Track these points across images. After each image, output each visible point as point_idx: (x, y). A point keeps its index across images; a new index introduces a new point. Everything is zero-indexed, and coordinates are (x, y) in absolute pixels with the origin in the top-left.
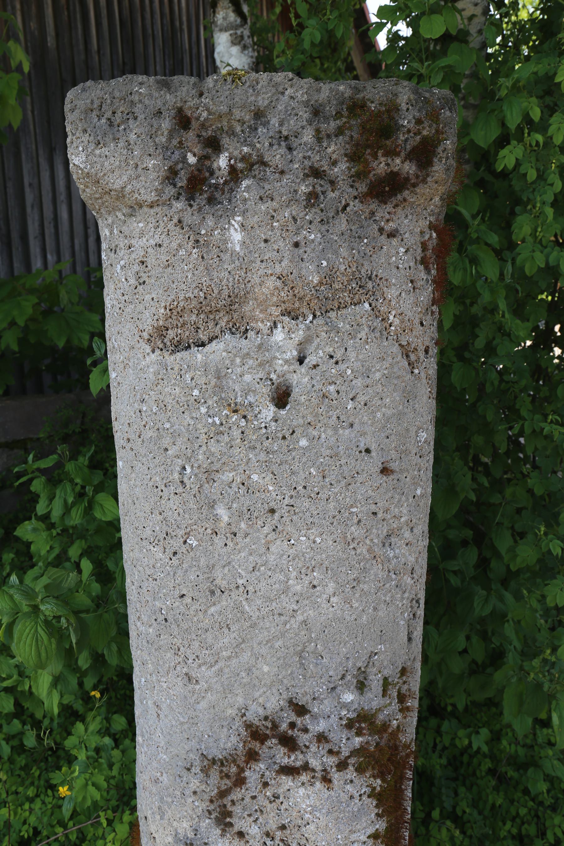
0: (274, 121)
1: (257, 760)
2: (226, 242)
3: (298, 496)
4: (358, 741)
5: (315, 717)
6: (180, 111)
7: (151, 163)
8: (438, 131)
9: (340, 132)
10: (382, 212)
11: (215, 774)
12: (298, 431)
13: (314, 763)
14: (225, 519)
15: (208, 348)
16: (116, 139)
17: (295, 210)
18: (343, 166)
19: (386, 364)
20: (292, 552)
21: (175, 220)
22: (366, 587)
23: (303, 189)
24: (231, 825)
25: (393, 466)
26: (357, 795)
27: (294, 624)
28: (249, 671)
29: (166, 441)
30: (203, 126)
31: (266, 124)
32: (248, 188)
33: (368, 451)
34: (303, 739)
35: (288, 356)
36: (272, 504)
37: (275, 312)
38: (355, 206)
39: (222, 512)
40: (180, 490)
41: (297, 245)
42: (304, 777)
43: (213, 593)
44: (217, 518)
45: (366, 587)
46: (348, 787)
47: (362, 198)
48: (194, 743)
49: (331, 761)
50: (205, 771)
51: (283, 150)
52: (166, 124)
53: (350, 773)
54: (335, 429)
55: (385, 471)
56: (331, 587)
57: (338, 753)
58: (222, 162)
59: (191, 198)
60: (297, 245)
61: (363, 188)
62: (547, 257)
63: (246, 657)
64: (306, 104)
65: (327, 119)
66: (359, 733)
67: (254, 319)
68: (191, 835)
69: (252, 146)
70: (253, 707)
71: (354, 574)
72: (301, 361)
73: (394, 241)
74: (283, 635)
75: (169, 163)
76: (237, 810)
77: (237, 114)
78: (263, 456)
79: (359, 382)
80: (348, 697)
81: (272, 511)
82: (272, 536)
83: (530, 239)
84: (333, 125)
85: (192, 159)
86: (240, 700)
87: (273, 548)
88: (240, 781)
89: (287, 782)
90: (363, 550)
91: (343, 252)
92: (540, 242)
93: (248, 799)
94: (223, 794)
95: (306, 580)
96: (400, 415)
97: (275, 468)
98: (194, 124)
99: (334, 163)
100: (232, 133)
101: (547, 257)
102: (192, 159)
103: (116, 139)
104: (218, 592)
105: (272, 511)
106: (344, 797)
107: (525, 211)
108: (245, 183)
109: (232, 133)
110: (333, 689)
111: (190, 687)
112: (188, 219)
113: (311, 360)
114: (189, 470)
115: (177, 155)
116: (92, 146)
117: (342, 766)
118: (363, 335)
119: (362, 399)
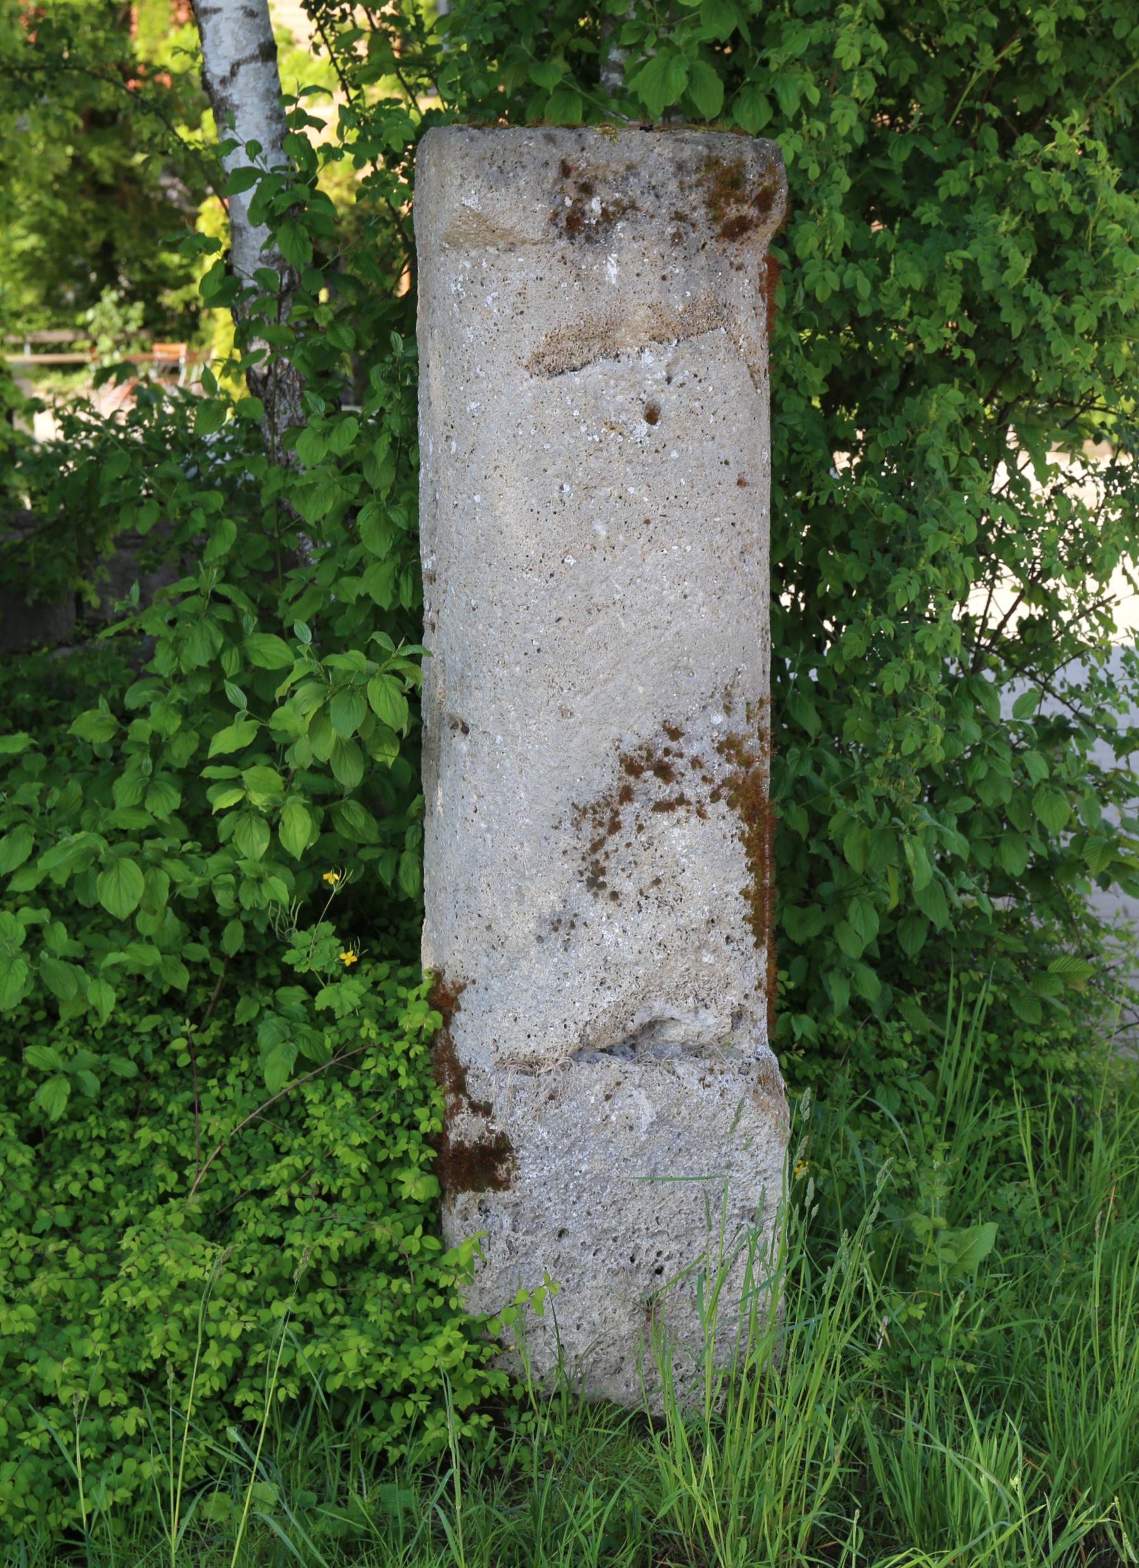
0: (645, 174)
1: (631, 800)
2: (603, 275)
3: (671, 505)
4: (728, 768)
5: (689, 741)
6: (563, 162)
7: (539, 207)
9: (699, 184)
10: (732, 248)
11: (587, 826)
12: (670, 445)
13: (689, 794)
14: (604, 533)
15: (584, 372)
16: (507, 185)
17: (663, 248)
18: (702, 211)
21: (559, 256)
23: (670, 230)
24: (603, 885)
25: (748, 478)
27: (669, 636)
28: (624, 694)
29: (545, 462)
30: (581, 175)
31: (637, 175)
32: (623, 230)
34: (680, 764)
35: (658, 376)
36: (648, 515)
37: (644, 337)
38: (712, 245)
39: (600, 528)
40: (559, 508)
41: (664, 278)
42: (681, 812)
46: (721, 823)
47: (718, 238)
48: (563, 794)
49: (706, 790)
50: (576, 824)
51: (652, 198)
53: (722, 806)
55: (741, 483)
58: (595, 205)
59: (572, 238)
60: (664, 278)
61: (718, 229)
62: (841, 276)
63: (622, 678)
64: (672, 160)
65: (689, 173)
66: (729, 761)
67: (623, 344)
68: (559, 908)
69: (625, 193)
71: (719, 584)
72: (669, 380)
76: (610, 864)
77: (613, 166)
78: (639, 469)
79: (719, 398)
80: (718, 719)
81: (647, 522)
82: (648, 546)
83: (818, 255)
84: (694, 178)
86: (614, 731)
87: (649, 559)
88: (615, 827)
89: (663, 820)
90: (726, 559)
92: (830, 258)
93: (622, 849)
94: (596, 846)
96: (750, 430)
97: (650, 479)
98: (574, 174)
99: (694, 209)
100: (605, 181)
101: (841, 276)
102: (568, 202)
103: (507, 185)
104: (594, 612)
105: (647, 522)
107: (807, 217)
108: (619, 225)
111: (564, 722)
112: (570, 256)
114: (567, 488)
116: (484, 191)
117: (715, 796)
118: (721, 356)
119: (721, 413)
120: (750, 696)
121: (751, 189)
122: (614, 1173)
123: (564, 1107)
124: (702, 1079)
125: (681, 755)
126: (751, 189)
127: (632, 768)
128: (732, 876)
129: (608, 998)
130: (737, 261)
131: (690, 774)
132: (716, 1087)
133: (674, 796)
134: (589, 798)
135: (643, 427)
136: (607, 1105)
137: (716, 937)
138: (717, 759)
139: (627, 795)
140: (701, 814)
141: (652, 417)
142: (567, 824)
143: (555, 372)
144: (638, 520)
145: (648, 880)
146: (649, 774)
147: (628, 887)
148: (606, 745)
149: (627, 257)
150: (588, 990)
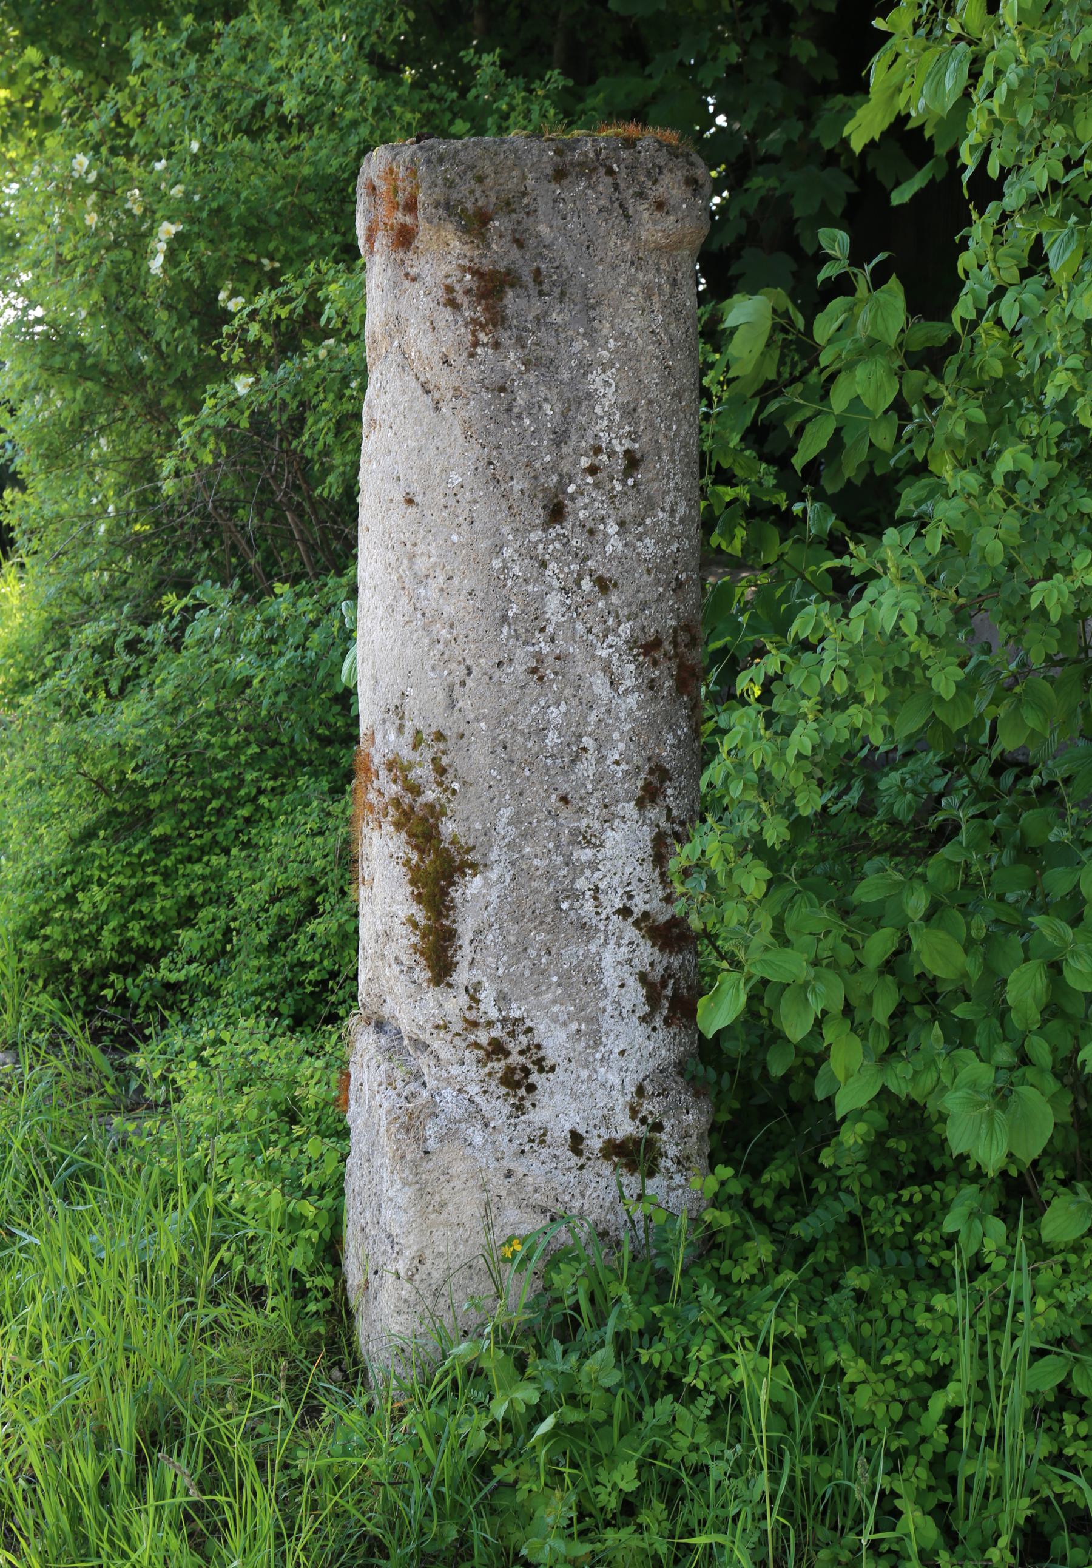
73: (417, 285)
120: (419, 723)
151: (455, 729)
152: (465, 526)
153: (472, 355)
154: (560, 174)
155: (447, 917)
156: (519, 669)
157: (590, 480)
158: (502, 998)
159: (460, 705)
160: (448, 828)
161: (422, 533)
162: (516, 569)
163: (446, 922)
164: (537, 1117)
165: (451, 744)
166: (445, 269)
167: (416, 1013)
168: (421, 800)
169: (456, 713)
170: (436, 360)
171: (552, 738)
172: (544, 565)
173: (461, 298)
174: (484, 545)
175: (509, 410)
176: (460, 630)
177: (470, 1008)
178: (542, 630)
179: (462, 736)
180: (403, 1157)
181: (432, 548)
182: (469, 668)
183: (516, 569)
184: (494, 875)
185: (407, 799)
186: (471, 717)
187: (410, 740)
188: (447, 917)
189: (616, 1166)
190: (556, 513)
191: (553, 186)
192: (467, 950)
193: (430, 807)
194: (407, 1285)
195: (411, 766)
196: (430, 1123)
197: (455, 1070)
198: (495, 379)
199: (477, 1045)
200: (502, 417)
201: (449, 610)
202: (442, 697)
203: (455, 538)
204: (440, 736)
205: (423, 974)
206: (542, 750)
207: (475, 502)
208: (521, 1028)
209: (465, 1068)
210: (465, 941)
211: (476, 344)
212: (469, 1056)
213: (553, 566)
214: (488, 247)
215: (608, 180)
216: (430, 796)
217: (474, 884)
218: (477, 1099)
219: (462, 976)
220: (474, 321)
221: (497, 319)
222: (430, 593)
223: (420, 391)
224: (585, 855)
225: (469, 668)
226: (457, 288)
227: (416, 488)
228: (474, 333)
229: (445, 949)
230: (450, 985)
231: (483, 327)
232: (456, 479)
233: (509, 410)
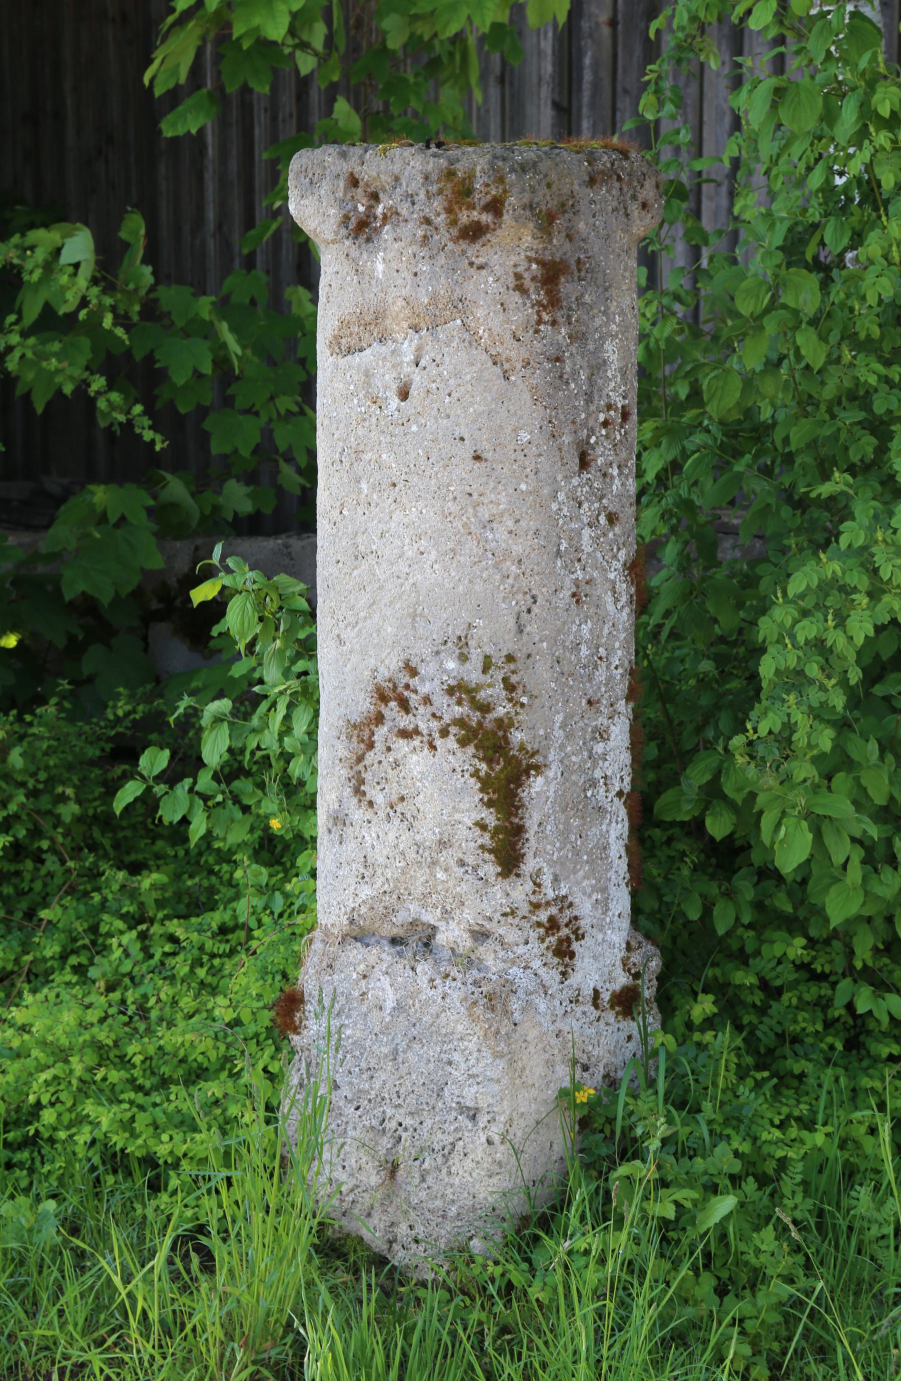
2: (373, 271)
5: (423, 680)
6: (352, 174)
7: (332, 211)
8: (505, 191)
9: (440, 192)
13: (423, 727)
17: (415, 248)
19: (475, 368)
20: (406, 520)
22: (462, 559)
23: (420, 233)
26: (459, 770)
30: (367, 185)
33: (462, 439)
34: (414, 699)
38: (450, 245)
42: (416, 742)
43: (356, 558)
44: (360, 491)
45: (462, 559)
47: (455, 240)
49: (435, 725)
51: (409, 204)
52: (342, 184)
53: (451, 743)
54: (436, 418)
56: (433, 555)
57: (441, 718)
61: (455, 232)
63: (376, 618)
66: (459, 703)
70: (382, 669)
71: (450, 545)
73: (484, 272)
74: (400, 597)
75: (343, 212)
78: (388, 439)
81: (394, 485)
82: (393, 506)
85: (361, 209)
88: (371, 746)
89: (402, 746)
91: (443, 280)
95: (416, 546)
98: (361, 184)
99: (438, 215)
102: (361, 209)
105: (394, 485)
106: (447, 768)
109: (384, 191)
110: (438, 653)
113: (423, 363)
115: (349, 206)
117: (444, 733)
118: (454, 344)
120: (489, 650)
121: (480, 198)
122: (368, 1043)
123: (336, 976)
124: (432, 980)
125: (415, 692)
126: (480, 198)
127: (383, 698)
128: (462, 806)
129: (366, 892)
130: (481, 261)
131: (422, 710)
132: (440, 990)
133: (411, 727)
134: (356, 718)
135: (394, 402)
136: (363, 982)
137: (448, 857)
138: (446, 699)
139: (379, 719)
140: (433, 747)
141: (404, 395)
142: (343, 737)
143: (350, 351)
144: (386, 482)
145: (394, 798)
146: (393, 704)
147: (380, 799)
148: (367, 673)
149: (390, 255)
150: (352, 880)
151: (525, 651)
152: (532, 476)
153: (537, 331)
154: (592, 182)
155: (516, 815)
156: (566, 594)
157: (604, 432)
158: (556, 879)
159: (529, 629)
160: (517, 736)
161: (492, 484)
162: (565, 511)
163: (516, 820)
164: (575, 979)
165: (520, 665)
166: (514, 259)
167: (484, 905)
168: (490, 716)
169: (525, 637)
170: (508, 336)
171: (584, 651)
172: (580, 504)
173: (528, 283)
174: (546, 491)
175: (561, 377)
176: (527, 565)
177: (534, 892)
178: (579, 560)
179: (529, 656)
180: (498, 1032)
181: (503, 498)
182: (534, 597)
183: (565, 511)
184: (551, 774)
185: (476, 716)
186: (537, 639)
187: (480, 666)
188: (516, 815)
189: (617, 1014)
190: (584, 463)
191: (588, 190)
192: (533, 842)
193: (499, 722)
194: (502, 1148)
195: (479, 688)
196: (514, 999)
197: (521, 950)
198: (552, 351)
199: (539, 924)
200: (558, 382)
201: (517, 549)
202: (512, 624)
203: (523, 487)
204: (510, 658)
205: (491, 869)
206: (579, 661)
207: (540, 455)
208: (566, 904)
209: (529, 946)
210: (530, 834)
211: (540, 322)
212: (533, 935)
213: (586, 505)
214: (551, 241)
215: (617, 185)
216: (500, 711)
217: (537, 785)
218: (539, 972)
219: (529, 865)
220: (539, 303)
221: (554, 301)
222: (500, 535)
223: (490, 363)
224: (599, 748)
225: (534, 597)
226: (526, 275)
227: (485, 447)
228: (538, 313)
229: (516, 844)
230: (518, 875)
231: (545, 308)
232: (525, 436)
233: (561, 377)
